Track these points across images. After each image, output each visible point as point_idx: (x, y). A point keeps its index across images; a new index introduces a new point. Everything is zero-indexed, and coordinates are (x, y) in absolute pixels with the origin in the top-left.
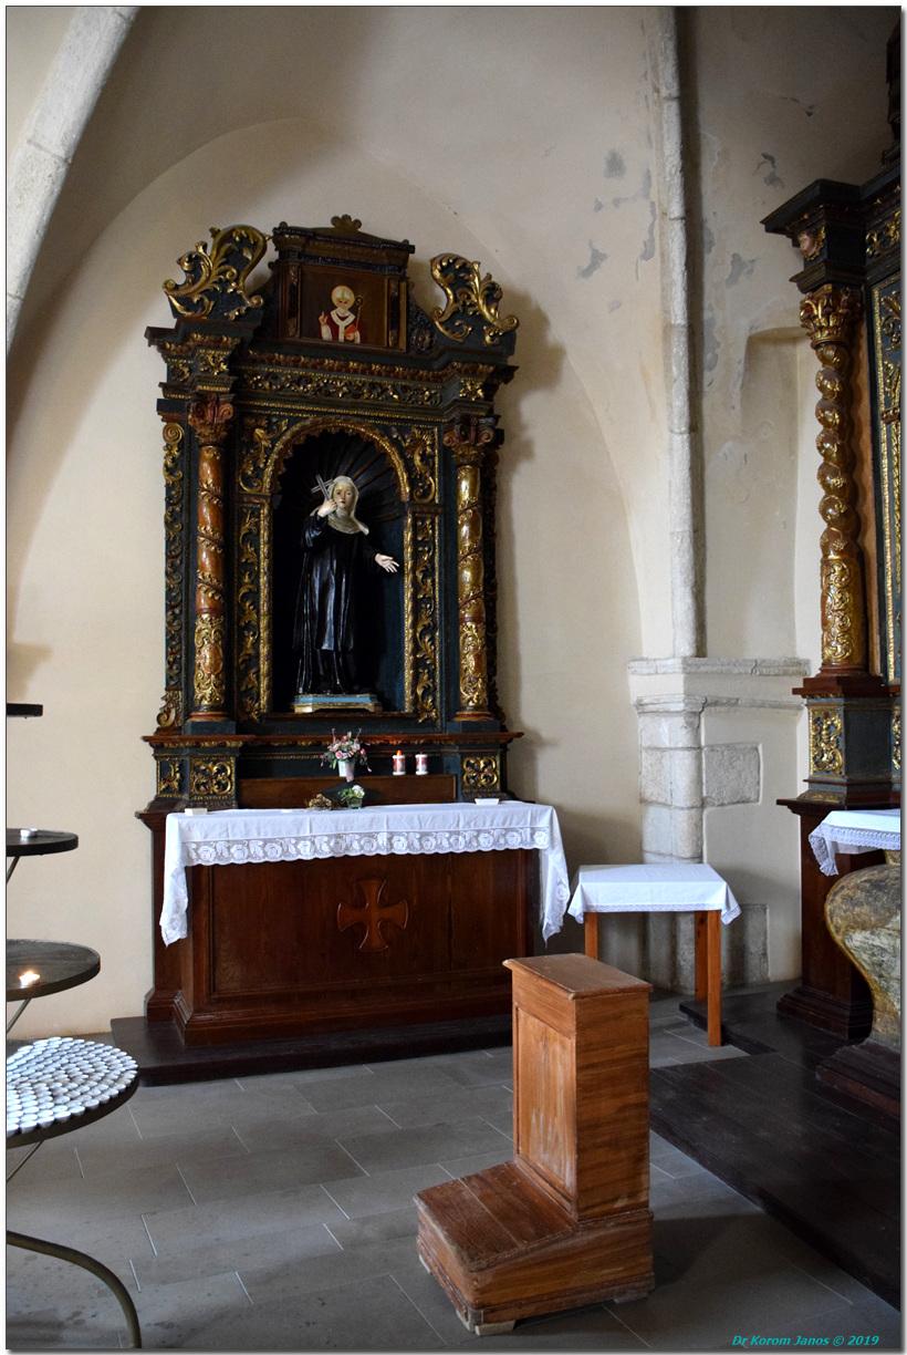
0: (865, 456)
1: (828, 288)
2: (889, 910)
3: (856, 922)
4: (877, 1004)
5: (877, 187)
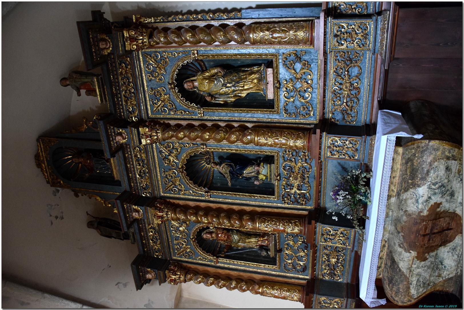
0: (227, 273)
1: (167, 272)
2: (401, 275)
3: (407, 291)
4: (440, 289)
5: (141, 248)
